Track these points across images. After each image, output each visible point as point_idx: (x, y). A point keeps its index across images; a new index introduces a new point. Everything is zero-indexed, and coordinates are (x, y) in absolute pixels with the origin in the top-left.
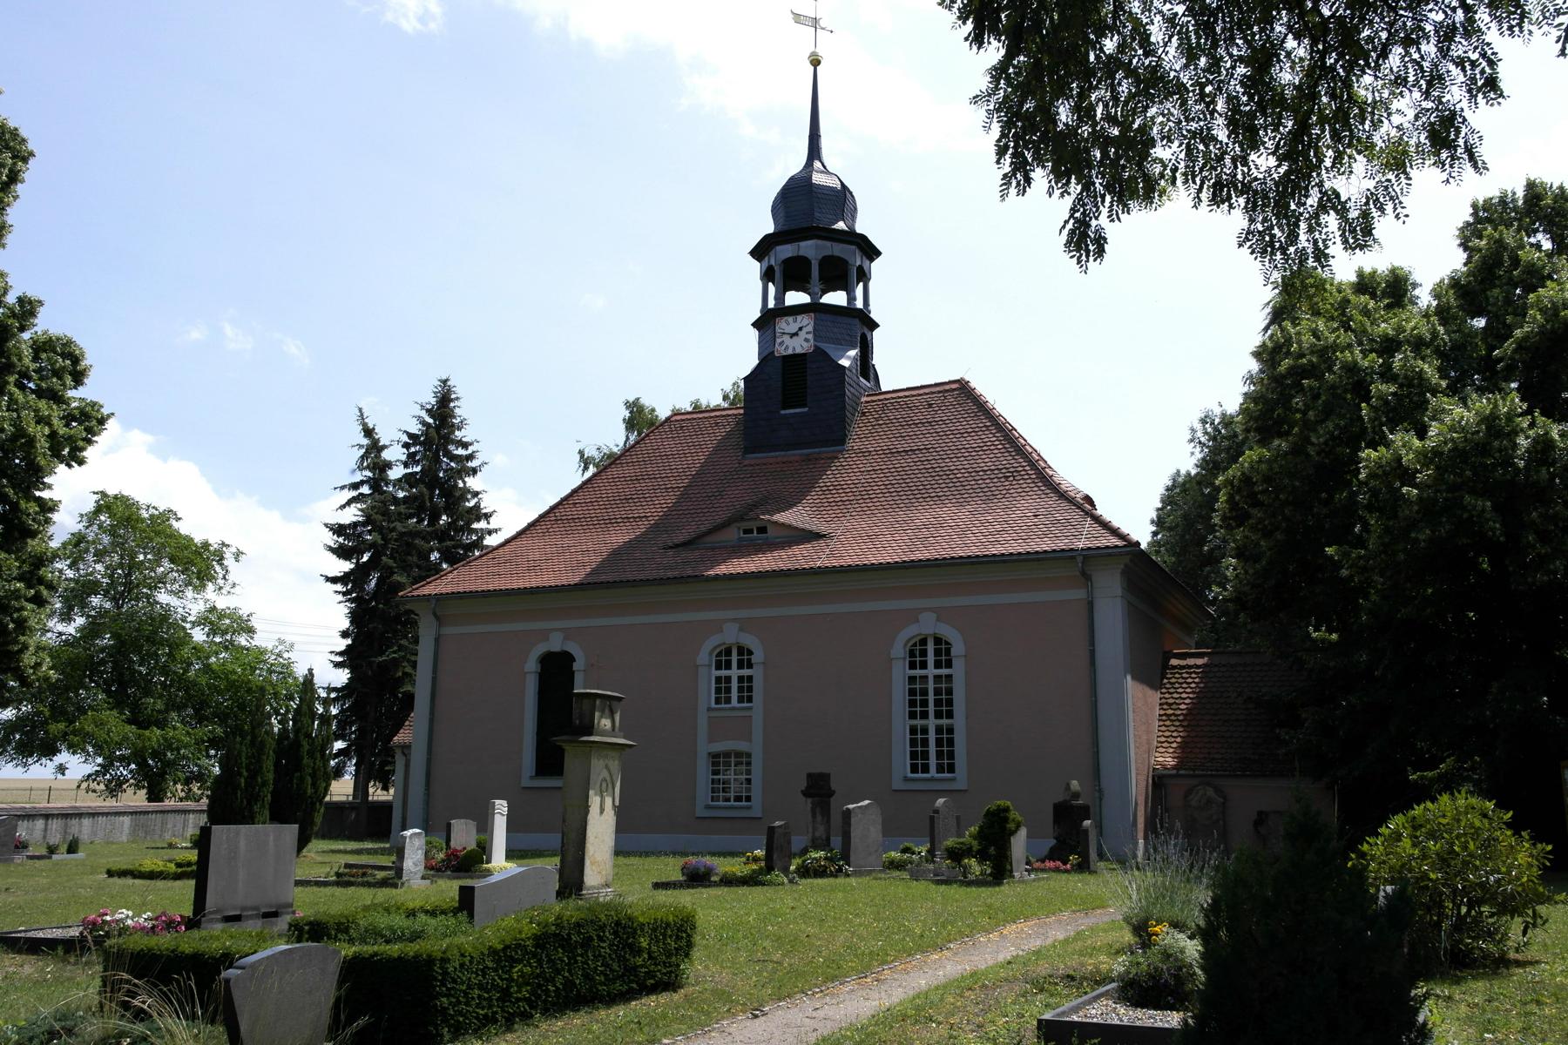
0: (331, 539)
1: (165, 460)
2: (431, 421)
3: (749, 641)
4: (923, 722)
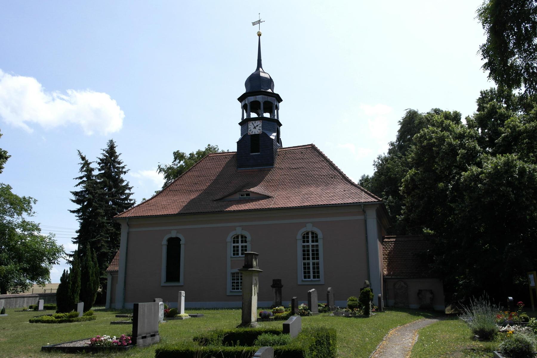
0: (74, 198)
2: (107, 155)
4: (308, 261)
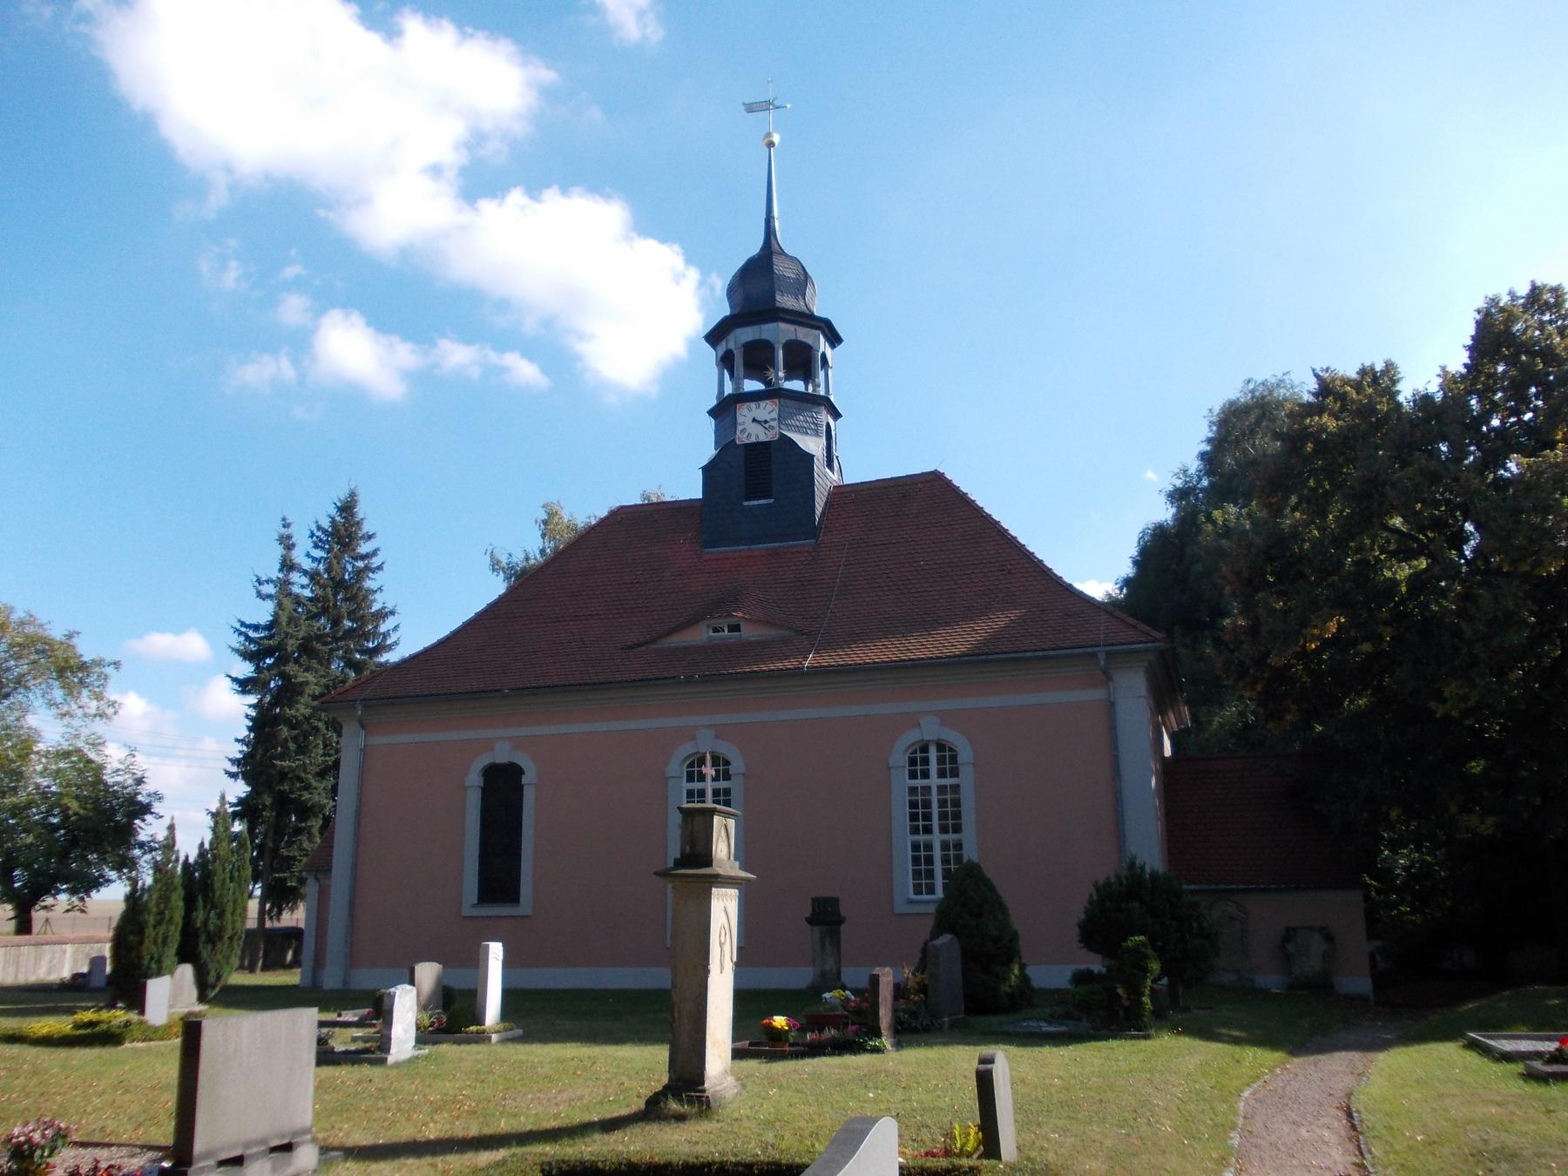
1: (392, 33)
3: (727, 750)
4: (928, 837)
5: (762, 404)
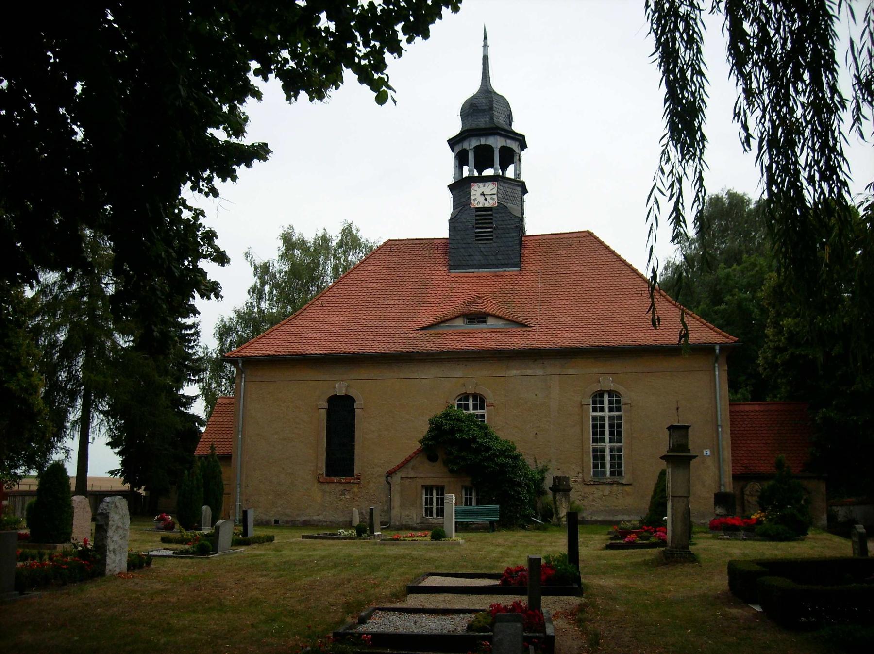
5: (487, 184)
